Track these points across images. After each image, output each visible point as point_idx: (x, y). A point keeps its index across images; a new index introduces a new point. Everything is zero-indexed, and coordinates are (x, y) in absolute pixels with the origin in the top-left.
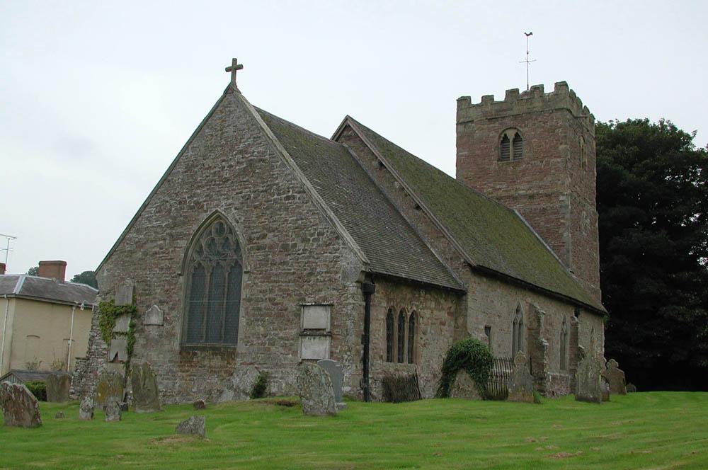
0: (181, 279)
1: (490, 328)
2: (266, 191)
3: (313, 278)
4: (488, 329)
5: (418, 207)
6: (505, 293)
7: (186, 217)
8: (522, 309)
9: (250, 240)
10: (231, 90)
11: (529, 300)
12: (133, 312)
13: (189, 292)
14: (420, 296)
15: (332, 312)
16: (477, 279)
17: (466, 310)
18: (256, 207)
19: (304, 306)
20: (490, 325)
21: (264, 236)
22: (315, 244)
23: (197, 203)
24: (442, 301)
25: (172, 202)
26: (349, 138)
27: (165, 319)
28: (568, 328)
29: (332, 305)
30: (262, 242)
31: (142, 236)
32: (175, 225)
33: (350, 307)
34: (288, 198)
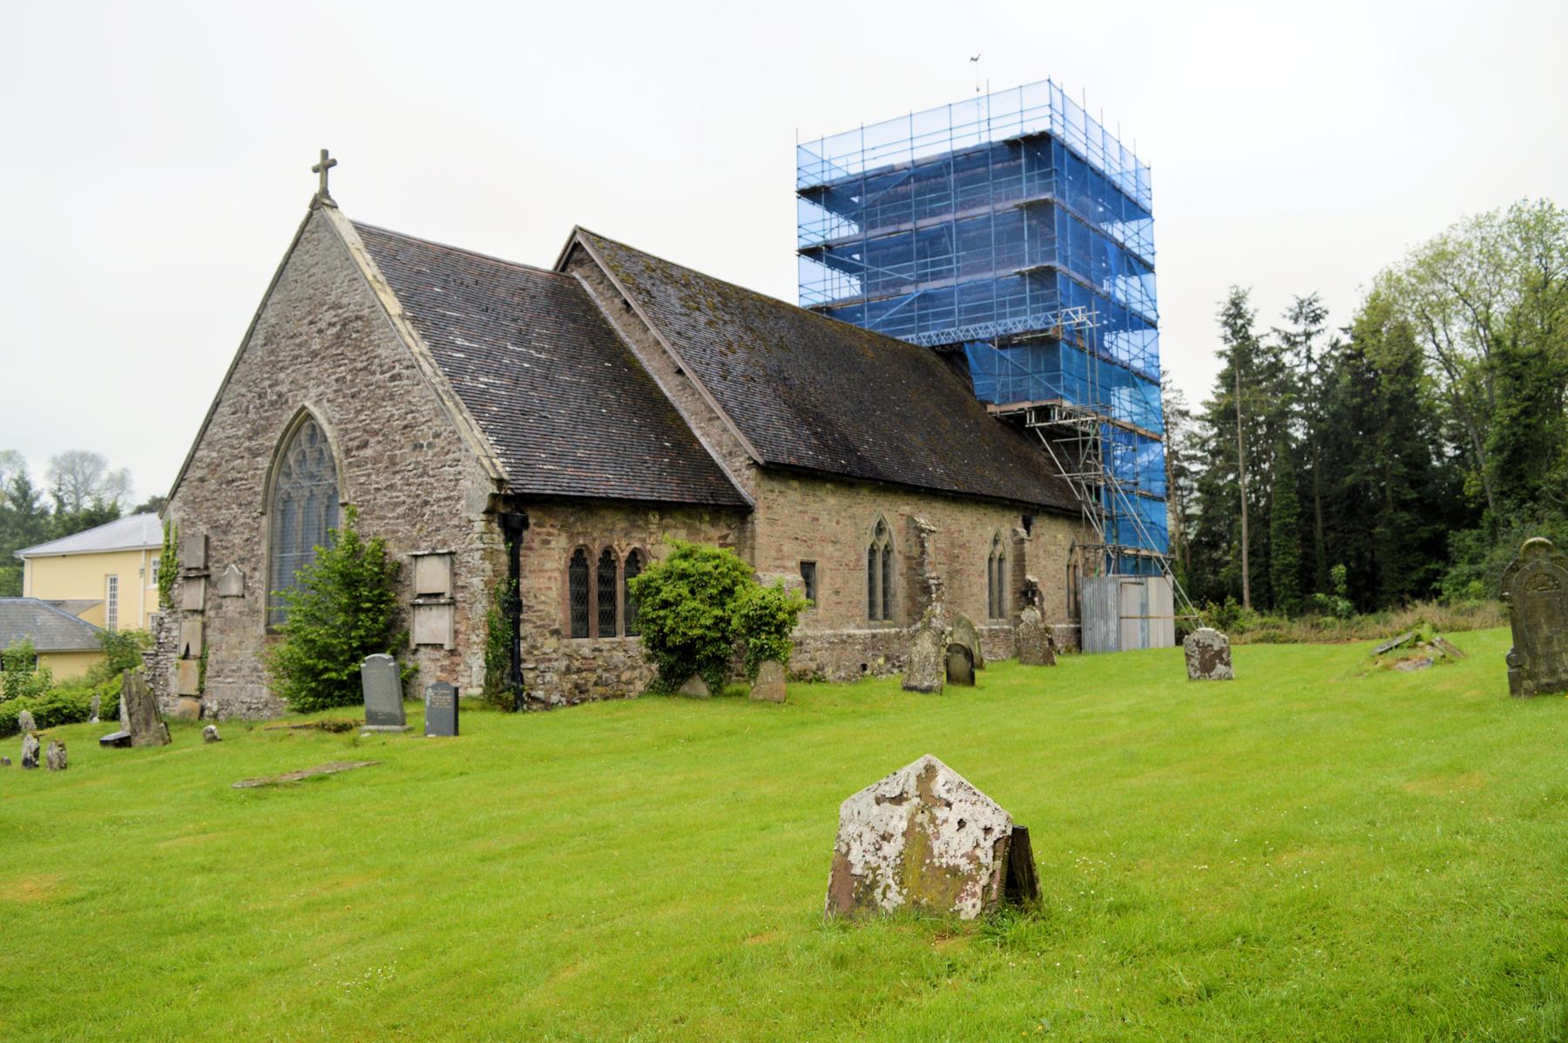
0: (264, 521)
1: (813, 564)
2: (365, 368)
3: (427, 510)
4: (807, 568)
5: (680, 372)
6: (846, 502)
7: (267, 419)
8: (889, 527)
9: (348, 451)
10: (322, 201)
11: (907, 509)
12: (203, 575)
13: (277, 540)
14: (647, 522)
15: (453, 563)
16: (777, 486)
17: (753, 537)
18: (353, 396)
19: (416, 557)
20: (812, 559)
21: (365, 445)
22: (430, 453)
23: (280, 395)
24: (706, 527)
25: (250, 396)
26: (580, 263)
27: (245, 587)
28: (1007, 549)
29: (451, 554)
30: (362, 453)
31: (214, 454)
32: (256, 433)
33: (477, 555)
34: (393, 378)
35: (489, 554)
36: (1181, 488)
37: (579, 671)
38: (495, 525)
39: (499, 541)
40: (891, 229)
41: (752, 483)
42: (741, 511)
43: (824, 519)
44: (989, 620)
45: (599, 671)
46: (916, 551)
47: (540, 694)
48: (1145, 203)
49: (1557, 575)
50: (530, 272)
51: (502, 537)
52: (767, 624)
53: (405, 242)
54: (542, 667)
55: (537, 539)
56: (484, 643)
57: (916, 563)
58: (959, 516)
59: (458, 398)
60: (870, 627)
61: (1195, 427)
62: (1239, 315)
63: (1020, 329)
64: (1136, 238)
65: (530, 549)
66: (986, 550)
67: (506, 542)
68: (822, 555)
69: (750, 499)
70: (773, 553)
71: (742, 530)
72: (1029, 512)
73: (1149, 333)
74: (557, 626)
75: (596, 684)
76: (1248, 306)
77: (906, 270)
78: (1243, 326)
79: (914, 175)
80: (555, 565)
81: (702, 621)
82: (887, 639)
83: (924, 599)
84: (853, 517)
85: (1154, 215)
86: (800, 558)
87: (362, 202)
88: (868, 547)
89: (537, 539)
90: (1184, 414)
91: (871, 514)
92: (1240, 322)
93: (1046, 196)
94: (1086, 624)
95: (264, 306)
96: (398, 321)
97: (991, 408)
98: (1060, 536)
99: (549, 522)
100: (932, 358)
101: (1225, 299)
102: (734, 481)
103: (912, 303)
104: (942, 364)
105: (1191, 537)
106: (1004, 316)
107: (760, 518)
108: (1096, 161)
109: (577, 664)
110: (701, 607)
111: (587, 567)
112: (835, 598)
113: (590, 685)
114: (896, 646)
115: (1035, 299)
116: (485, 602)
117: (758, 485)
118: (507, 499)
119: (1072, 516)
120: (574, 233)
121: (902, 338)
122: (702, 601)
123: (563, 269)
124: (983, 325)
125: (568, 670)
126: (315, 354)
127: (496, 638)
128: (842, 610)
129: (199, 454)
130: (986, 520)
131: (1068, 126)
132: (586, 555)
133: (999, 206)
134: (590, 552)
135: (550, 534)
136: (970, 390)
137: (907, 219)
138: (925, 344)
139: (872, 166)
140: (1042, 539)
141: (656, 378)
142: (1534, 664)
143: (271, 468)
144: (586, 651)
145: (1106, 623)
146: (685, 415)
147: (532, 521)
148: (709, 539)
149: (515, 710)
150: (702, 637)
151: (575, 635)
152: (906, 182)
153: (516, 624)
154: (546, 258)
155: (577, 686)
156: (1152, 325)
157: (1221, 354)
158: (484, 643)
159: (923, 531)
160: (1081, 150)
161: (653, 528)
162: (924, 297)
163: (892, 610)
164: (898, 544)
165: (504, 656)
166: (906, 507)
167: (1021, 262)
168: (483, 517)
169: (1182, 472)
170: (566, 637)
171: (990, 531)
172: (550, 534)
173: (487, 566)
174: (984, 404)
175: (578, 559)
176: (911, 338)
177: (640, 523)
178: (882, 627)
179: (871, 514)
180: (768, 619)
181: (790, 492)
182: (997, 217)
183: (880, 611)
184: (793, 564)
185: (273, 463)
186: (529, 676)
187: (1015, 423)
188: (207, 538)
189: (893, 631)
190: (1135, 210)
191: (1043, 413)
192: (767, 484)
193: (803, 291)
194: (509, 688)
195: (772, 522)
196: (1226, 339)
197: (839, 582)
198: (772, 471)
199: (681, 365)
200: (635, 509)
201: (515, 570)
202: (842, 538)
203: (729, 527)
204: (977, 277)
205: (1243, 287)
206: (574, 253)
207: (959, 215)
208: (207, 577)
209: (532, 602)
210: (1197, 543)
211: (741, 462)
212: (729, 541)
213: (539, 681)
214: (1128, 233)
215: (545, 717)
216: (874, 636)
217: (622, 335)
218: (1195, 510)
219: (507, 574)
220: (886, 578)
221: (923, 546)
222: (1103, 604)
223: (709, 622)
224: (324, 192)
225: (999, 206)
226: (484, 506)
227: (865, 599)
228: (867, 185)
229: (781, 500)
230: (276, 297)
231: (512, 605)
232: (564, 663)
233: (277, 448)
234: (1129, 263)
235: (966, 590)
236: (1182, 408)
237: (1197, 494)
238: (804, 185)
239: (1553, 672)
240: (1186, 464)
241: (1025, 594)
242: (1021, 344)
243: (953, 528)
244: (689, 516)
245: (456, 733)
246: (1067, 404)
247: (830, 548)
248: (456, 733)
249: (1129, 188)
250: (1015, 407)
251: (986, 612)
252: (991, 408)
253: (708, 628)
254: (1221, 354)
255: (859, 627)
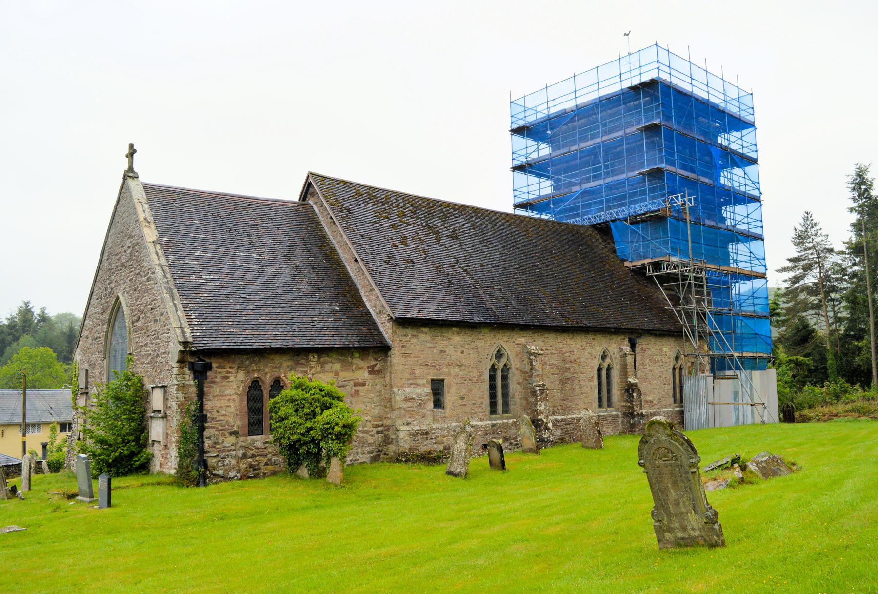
5: (356, 260)
9: (133, 322)
10: (130, 174)
11: (523, 340)
14: (308, 361)
15: (165, 392)
20: (441, 378)
29: (164, 387)
35: (182, 387)
36: (832, 300)
37: (253, 456)
38: (186, 369)
39: (189, 378)
40: (565, 150)
41: (390, 331)
42: (384, 349)
43: (450, 351)
44: (598, 410)
45: (269, 456)
46: (528, 368)
47: (221, 472)
48: (746, 116)
49: (674, 450)
50: (273, 205)
51: (192, 376)
52: (331, 434)
53: (184, 193)
54: (222, 455)
55: (219, 376)
56: (177, 442)
57: (528, 375)
58: (570, 342)
59: (175, 291)
60: (490, 419)
61: (837, 259)
62: (863, 182)
63: (644, 210)
64: (739, 142)
65: (214, 382)
66: (596, 363)
67: (195, 378)
68: (449, 374)
69: (389, 342)
70: (407, 375)
71: (385, 361)
72: (634, 335)
73: (753, 206)
74: (235, 429)
75: (266, 464)
76: (868, 176)
77: (575, 176)
78: (866, 190)
79: (577, 115)
80: (233, 392)
81: (299, 431)
82: (506, 427)
83: (532, 400)
84: (476, 348)
85: (756, 125)
86: (430, 377)
87: (151, 172)
88: (489, 367)
89: (219, 376)
90: (831, 251)
91: (491, 345)
92: (863, 187)
93: (657, 121)
94: (687, 408)
95: (107, 237)
96: (151, 247)
97: (627, 264)
98: (665, 349)
99: (228, 365)
100: (591, 232)
101: (853, 172)
102: (382, 329)
103: (578, 197)
104: (598, 236)
105: (842, 332)
106: (636, 202)
107: (396, 356)
108: (700, 92)
109: (252, 452)
110: (299, 421)
111: (262, 391)
112: (461, 402)
113: (262, 465)
114: (513, 431)
115: (652, 190)
116: (178, 417)
117: (394, 332)
118: (192, 354)
119: (677, 334)
120: (308, 177)
121: (571, 221)
122: (301, 417)
123: (304, 199)
124: (621, 209)
125: (245, 456)
126: (123, 265)
127: (186, 439)
128: (467, 409)
129: (87, 322)
130: (593, 342)
131: (673, 72)
132: (260, 383)
133: (628, 131)
134: (263, 382)
135: (228, 373)
136: (614, 251)
137: (574, 142)
138: (587, 223)
139: (553, 111)
140: (648, 352)
141: (346, 264)
142: (670, 521)
143: (107, 332)
144: (259, 444)
145: (700, 408)
146: (359, 287)
147: (214, 365)
148: (361, 368)
149: (198, 485)
150: (299, 441)
151: (251, 433)
152: (572, 120)
153: (202, 429)
154: (294, 195)
155: (251, 466)
156: (757, 200)
157: (851, 210)
158: (177, 442)
159: (531, 354)
160: (686, 87)
161: (313, 364)
162: (585, 193)
163: (511, 407)
164: (514, 364)
165: (193, 450)
166: (522, 339)
167: (642, 166)
168: (177, 365)
169: (834, 289)
170: (244, 435)
171: (598, 350)
172: (228, 373)
173: (180, 395)
174: (623, 260)
175: (255, 386)
176: (578, 221)
177: (303, 361)
178: (500, 419)
179: (491, 345)
180: (330, 431)
181: (421, 335)
182: (627, 137)
183: (500, 408)
184: (425, 381)
185: (108, 328)
186: (212, 462)
187: (640, 272)
188: (87, 371)
189: (511, 421)
190: (740, 124)
191: (657, 266)
192: (401, 331)
193: (516, 193)
194: (197, 471)
195: (406, 355)
196: (854, 199)
197: (464, 391)
198: (402, 323)
199: (357, 257)
200: (299, 353)
201: (201, 395)
202: (466, 363)
203: (376, 359)
204: (616, 178)
205: (864, 163)
206: (307, 190)
207: (605, 138)
208: (87, 393)
209: (216, 415)
210: (846, 335)
211: (385, 318)
212: (376, 368)
213: (220, 464)
214: (732, 139)
215: (224, 485)
216: (493, 425)
217: (331, 238)
218: (845, 314)
219: (196, 399)
220: (505, 386)
221: (532, 365)
222: (697, 394)
223: (303, 431)
224: (131, 169)
225: (628, 131)
226: (176, 358)
227: (487, 401)
228: (551, 124)
229: (414, 341)
230: (112, 231)
231: (200, 419)
232: (240, 453)
233: (109, 320)
234: (732, 159)
235: (578, 391)
236: (827, 247)
237: (844, 304)
238: (515, 126)
239: (684, 529)
240: (835, 283)
241: (627, 390)
242: (643, 221)
243: (564, 350)
244: (342, 355)
245: (109, 505)
246: (674, 259)
247: (456, 369)
248: (109, 505)
249: (733, 109)
250: (639, 263)
251: (596, 404)
252: (627, 264)
253: (303, 435)
254: (851, 210)
255: (481, 420)
